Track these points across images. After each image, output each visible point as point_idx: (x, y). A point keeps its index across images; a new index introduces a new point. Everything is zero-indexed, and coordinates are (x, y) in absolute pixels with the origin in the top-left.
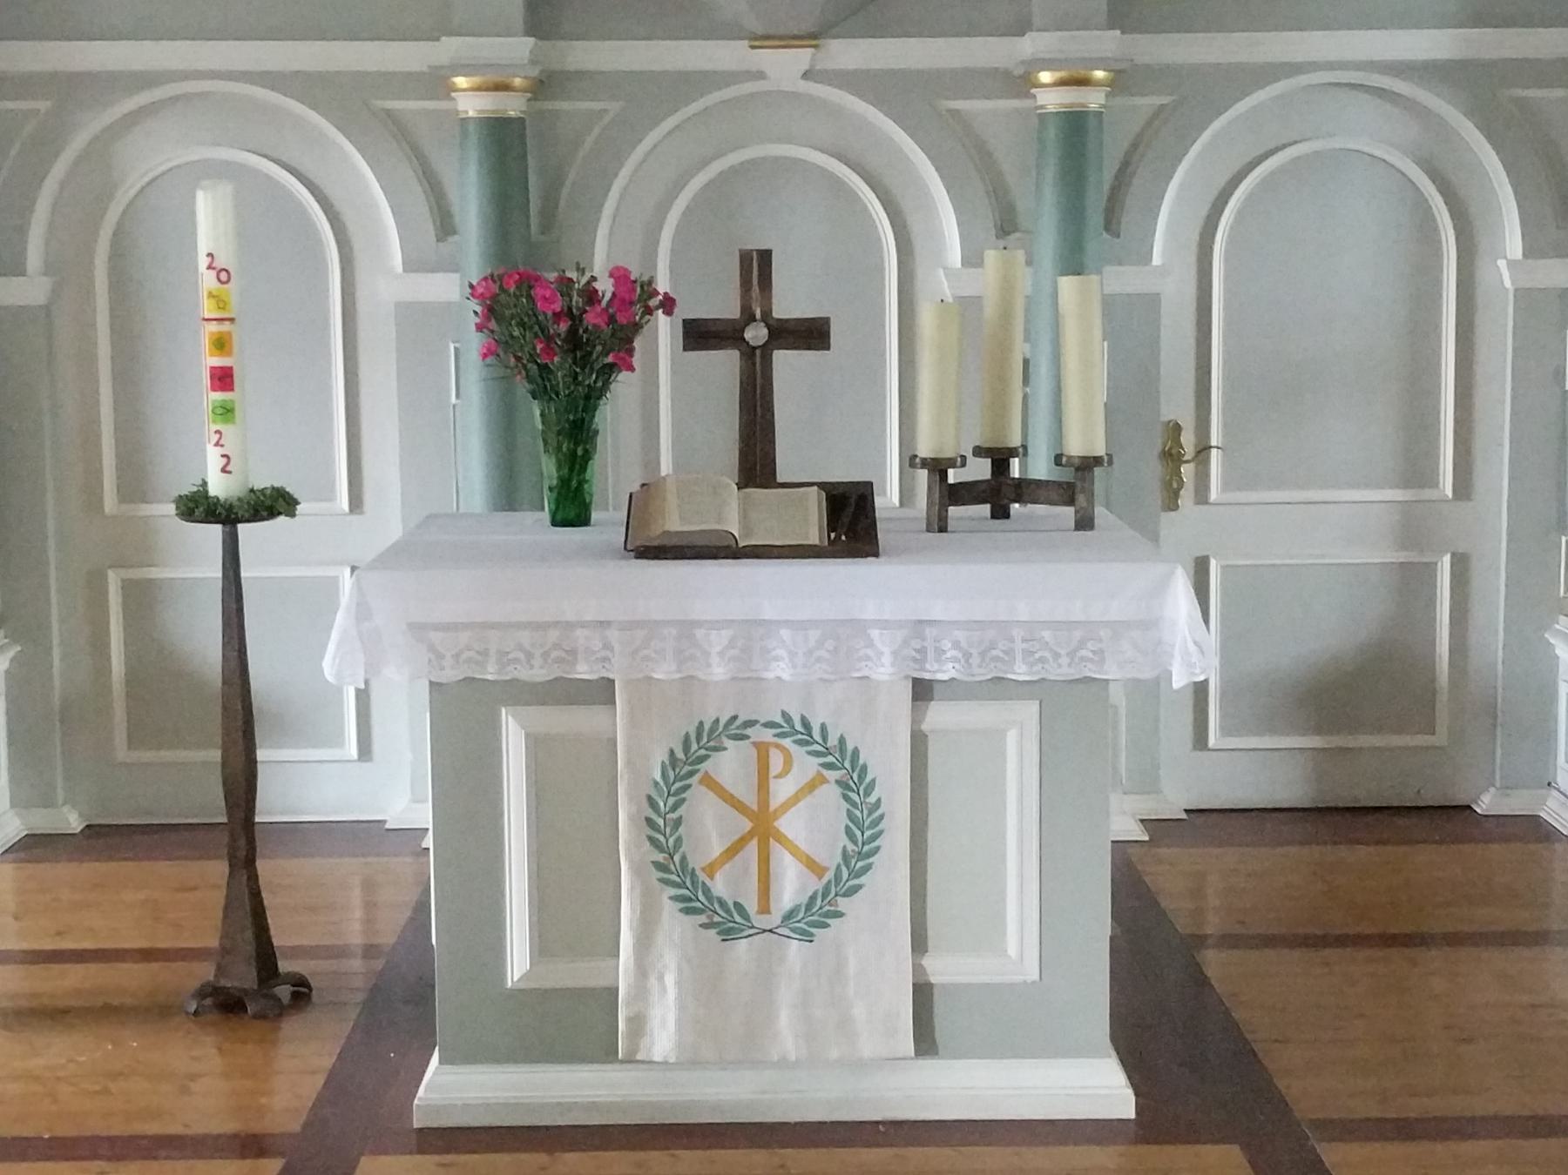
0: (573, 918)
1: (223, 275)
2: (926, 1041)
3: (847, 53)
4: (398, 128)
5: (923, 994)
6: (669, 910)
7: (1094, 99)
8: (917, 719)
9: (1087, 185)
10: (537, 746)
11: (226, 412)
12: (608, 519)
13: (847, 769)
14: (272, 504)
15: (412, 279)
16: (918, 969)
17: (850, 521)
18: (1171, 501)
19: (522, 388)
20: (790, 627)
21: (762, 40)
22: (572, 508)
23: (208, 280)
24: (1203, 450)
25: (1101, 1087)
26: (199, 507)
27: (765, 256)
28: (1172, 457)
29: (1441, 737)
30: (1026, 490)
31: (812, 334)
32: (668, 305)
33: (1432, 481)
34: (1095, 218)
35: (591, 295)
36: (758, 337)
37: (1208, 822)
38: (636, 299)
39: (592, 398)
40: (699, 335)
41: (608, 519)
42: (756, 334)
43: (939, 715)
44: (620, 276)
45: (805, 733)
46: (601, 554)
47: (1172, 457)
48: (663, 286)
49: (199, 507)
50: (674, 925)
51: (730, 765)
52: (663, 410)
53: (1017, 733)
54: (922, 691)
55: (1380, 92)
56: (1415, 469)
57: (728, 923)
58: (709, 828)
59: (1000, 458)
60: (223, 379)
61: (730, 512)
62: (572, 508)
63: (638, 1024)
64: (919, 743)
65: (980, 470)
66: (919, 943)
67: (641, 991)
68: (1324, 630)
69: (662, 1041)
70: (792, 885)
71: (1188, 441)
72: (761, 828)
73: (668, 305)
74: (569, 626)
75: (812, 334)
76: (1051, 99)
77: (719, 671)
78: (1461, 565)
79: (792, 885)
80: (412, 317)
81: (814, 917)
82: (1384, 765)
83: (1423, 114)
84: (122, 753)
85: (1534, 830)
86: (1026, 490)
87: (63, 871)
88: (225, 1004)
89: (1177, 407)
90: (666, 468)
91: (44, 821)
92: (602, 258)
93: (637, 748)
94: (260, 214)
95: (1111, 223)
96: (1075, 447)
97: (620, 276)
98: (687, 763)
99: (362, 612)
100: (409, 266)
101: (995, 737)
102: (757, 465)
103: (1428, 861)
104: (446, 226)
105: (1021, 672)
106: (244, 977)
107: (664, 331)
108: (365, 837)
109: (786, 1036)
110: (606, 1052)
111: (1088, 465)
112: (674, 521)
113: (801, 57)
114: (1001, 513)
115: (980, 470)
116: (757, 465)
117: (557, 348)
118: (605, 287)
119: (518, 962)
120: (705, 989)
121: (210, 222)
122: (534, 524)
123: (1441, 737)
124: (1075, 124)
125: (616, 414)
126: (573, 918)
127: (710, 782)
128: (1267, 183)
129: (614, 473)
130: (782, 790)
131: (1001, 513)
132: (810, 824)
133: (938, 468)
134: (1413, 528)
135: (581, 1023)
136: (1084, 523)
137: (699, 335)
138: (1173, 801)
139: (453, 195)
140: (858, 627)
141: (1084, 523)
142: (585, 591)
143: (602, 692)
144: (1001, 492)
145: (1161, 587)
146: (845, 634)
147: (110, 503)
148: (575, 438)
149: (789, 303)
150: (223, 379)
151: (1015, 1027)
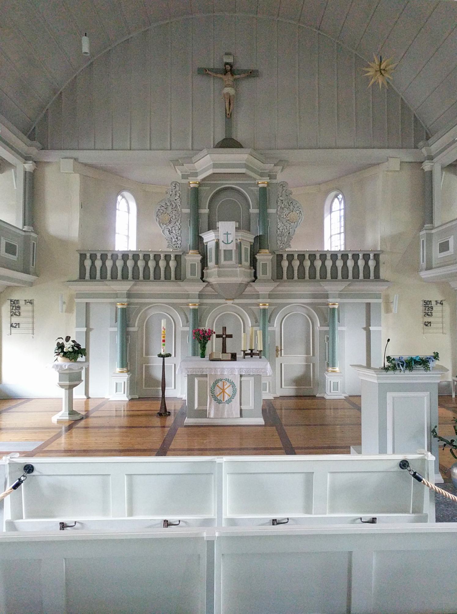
0: (203, 401)
1: (164, 329)
2: (241, 416)
3: (237, 301)
4: (182, 309)
5: (241, 410)
6: (213, 400)
7: (267, 307)
8: (240, 379)
9: (265, 317)
10: (199, 382)
11: (164, 345)
12: (207, 357)
13: (233, 384)
14: (169, 355)
15: (184, 328)
16: (240, 408)
17: (234, 357)
18: (277, 356)
19: (197, 342)
20: (229, 369)
21: (227, 299)
22: (203, 356)
23: (163, 330)
24: (281, 350)
25: (260, 421)
26: (160, 356)
27: (225, 327)
28: (277, 350)
29: (312, 387)
30: (254, 354)
31: (231, 336)
32: (214, 333)
33: (310, 354)
34: (267, 323)
35: (206, 331)
36: (224, 336)
37: (282, 397)
38: (211, 332)
39: (206, 343)
40: (218, 336)
41: (207, 357)
42: (224, 336)
43: (243, 379)
44: (209, 330)
45: (228, 380)
46: (207, 361)
47: (277, 350)
48: (214, 331)
49: (160, 356)
50: (213, 402)
51: (220, 384)
52: (214, 345)
53: (251, 380)
54: (241, 376)
55: (303, 307)
56: (307, 353)
57: (219, 402)
58: (218, 391)
59: (252, 350)
60: (164, 341)
61: (221, 356)
62: (203, 356)
63: (209, 413)
64: (241, 382)
65: (250, 352)
66: (241, 405)
67: (210, 410)
68: (298, 372)
69: (212, 416)
70: (227, 398)
71: (279, 349)
72: (223, 391)
73: (214, 333)
74: (203, 368)
75: (231, 336)
76: (262, 307)
77: (219, 373)
78: (314, 365)
79: (227, 398)
80: (183, 332)
81: (229, 401)
82: (305, 390)
83: (307, 309)
84: (144, 388)
85: (323, 398)
86: (254, 354)
87: (136, 402)
88: (160, 414)
89: (278, 344)
90: (214, 351)
91: (134, 397)
92: (206, 327)
93: (210, 382)
94: (168, 323)
95: (269, 322)
96: (259, 349)
97: (209, 330)
98: (216, 383)
99: (180, 367)
100: (183, 326)
101: (249, 381)
102: (224, 351)
103: (309, 401)
104: (187, 322)
105: (251, 374)
106: (163, 411)
107: (214, 335)
108: (175, 398)
109: (226, 415)
110: (206, 417)
111: (261, 351)
112: (214, 357)
113: (231, 301)
114: (252, 357)
115: (250, 352)
116: (224, 351)
117: (202, 338)
118: (207, 331)
119: (196, 406)
120: (217, 410)
121: (163, 323)
122: (199, 358)
123: (312, 387)
124: (264, 310)
125: (208, 345)
126: (203, 401)
127: (218, 386)
128: (288, 317)
129: (208, 351)
130: (226, 387)
131: (252, 357)
132: (229, 391)
133: (244, 351)
134: (307, 360)
135: (203, 413)
136: (260, 358)
137: (218, 336)
138: (278, 394)
139: (189, 317)
140: (234, 368)
141: (260, 358)
142: (205, 364)
143: (206, 376)
144: (252, 354)
145: (267, 364)
146: (233, 369)
147: (144, 356)
148: (204, 348)
149: (228, 332)
150: (164, 341)
151: (251, 414)
